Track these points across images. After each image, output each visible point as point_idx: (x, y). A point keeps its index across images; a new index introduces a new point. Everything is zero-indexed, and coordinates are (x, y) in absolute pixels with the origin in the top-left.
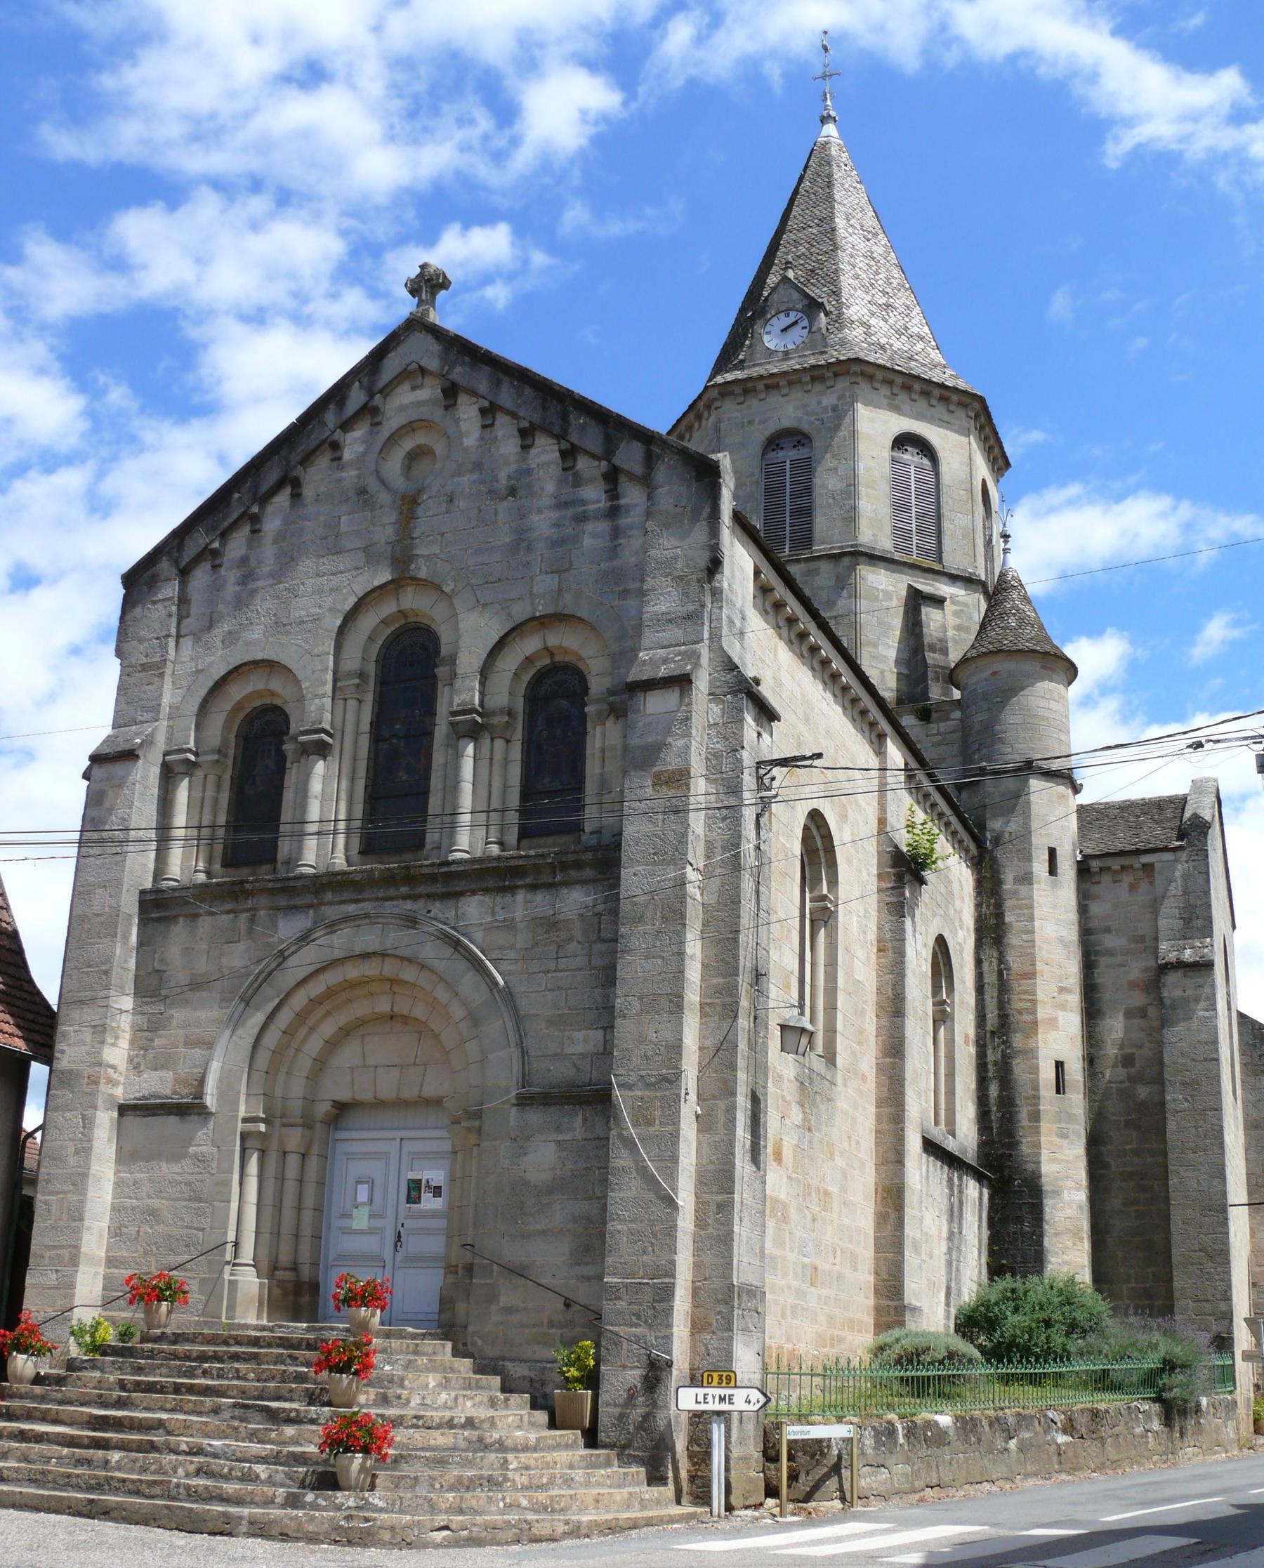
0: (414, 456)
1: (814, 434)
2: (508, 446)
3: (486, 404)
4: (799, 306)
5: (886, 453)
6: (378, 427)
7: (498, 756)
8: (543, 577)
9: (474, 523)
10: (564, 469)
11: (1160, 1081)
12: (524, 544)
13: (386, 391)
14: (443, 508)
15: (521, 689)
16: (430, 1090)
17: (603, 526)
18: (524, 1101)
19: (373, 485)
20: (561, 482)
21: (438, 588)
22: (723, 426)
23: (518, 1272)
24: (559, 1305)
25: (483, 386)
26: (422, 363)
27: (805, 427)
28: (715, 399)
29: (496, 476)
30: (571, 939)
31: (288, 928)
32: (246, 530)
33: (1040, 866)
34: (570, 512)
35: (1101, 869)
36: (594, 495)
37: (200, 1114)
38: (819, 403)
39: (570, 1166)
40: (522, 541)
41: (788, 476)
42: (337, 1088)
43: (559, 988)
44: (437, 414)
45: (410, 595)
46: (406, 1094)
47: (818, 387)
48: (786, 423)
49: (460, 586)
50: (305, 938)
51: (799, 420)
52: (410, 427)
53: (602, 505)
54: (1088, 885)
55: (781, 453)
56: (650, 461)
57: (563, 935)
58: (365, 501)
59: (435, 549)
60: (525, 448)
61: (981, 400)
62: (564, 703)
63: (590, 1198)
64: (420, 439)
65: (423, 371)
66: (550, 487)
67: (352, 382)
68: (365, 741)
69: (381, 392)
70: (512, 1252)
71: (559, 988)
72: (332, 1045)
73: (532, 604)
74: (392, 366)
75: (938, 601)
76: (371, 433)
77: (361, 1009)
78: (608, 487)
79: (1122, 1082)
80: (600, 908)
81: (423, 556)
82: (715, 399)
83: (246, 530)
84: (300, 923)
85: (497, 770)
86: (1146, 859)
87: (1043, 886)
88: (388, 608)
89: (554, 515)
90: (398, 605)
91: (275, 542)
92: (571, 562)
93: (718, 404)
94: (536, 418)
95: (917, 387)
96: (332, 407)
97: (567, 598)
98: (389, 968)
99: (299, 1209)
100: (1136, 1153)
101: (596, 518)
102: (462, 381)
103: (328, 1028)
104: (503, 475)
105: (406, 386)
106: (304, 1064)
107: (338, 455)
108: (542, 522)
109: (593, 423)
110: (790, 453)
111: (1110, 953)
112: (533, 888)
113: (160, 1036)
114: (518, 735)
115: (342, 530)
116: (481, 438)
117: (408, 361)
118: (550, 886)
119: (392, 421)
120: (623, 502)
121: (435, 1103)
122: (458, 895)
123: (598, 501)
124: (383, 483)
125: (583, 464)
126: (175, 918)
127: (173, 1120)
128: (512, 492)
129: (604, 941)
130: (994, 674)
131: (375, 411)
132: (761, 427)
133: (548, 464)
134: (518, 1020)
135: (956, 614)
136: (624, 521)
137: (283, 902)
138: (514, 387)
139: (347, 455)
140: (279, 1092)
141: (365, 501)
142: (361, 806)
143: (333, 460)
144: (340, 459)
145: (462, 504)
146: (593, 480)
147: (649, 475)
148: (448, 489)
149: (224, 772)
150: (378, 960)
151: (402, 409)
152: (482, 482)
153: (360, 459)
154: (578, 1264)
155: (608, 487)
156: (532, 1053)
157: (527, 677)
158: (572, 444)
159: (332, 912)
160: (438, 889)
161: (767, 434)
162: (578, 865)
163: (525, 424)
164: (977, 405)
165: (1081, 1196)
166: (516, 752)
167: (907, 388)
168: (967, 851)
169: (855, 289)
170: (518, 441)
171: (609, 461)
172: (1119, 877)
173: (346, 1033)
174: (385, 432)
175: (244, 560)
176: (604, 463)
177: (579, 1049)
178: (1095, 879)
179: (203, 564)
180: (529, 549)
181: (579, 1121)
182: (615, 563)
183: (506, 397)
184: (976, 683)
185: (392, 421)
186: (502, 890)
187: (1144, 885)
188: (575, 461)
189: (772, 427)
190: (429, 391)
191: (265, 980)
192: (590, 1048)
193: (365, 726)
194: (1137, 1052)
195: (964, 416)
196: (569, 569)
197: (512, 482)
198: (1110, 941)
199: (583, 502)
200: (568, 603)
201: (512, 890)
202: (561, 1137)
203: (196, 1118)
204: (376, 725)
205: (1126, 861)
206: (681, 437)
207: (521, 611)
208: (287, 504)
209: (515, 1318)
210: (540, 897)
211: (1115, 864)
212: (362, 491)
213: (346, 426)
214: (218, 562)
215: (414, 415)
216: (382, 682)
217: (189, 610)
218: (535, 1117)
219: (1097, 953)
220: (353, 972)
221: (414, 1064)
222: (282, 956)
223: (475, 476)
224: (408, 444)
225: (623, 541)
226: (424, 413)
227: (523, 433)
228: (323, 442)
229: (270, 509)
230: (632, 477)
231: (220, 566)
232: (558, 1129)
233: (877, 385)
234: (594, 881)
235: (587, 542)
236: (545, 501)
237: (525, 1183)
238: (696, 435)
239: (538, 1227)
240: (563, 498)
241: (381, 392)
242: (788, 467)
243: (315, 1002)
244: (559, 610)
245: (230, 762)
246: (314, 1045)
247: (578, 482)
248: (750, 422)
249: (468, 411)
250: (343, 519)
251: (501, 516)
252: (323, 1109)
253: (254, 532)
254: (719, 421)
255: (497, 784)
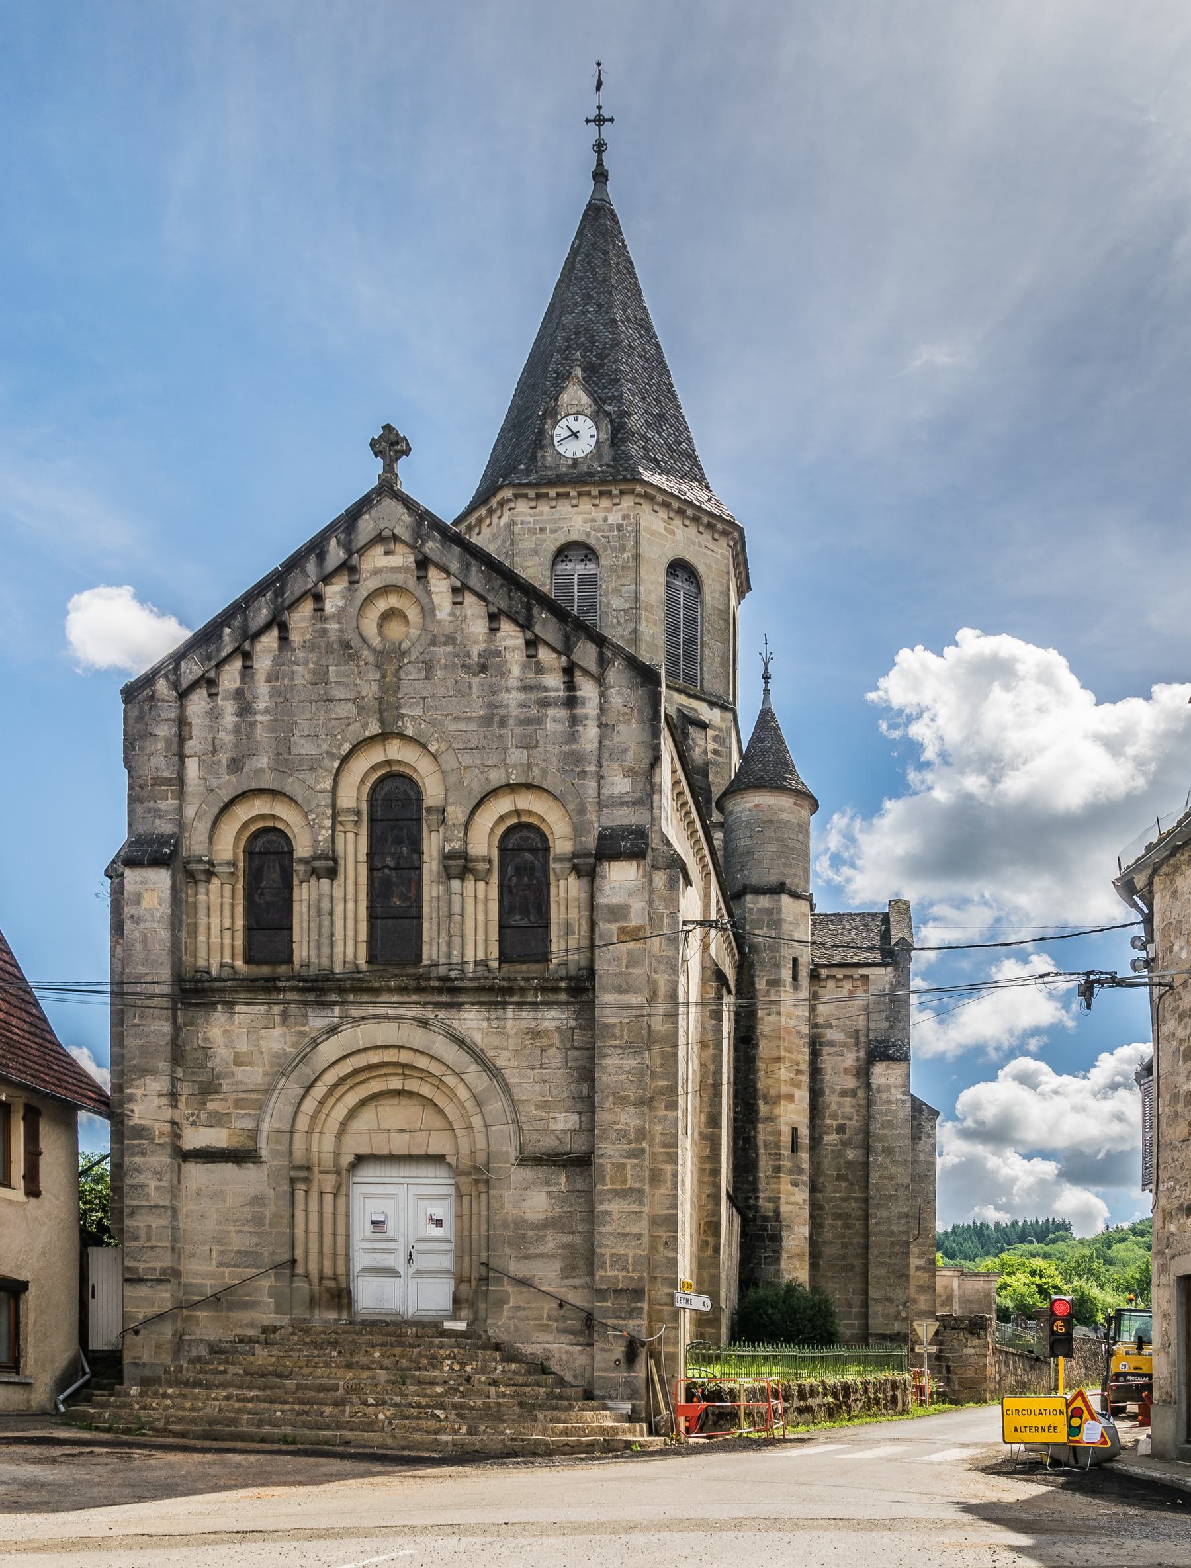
0: (389, 615)
1: (600, 551)
2: (479, 627)
3: (458, 583)
4: (588, 412)
5: (662, 578)
6: (356, 586)
7: (481, 896)
8: (514, 750)
9: (451, 693)
10: (528, 656)
11: (867, 1149)
12: (496, 719)
13: (362, 551)
14: (423, 675)
15: (496, 842)
16: (433, 1150)
17: (563, 713)
18: (522, 1162)
19: (356, 643)
20: (525, 667)
21: (425, 747)
22: (517, 529)
23: (523, 1282)
24: (555, 1305)
25: (454, 566)
26: (396, 531)
27: (592, 542)
28: (509, 500)
29: (468, 652)
30: (552, 1045)
31: (317, 1021)
32: (238, 664)
33: (786, 974)
34: (533, 696)
35: (829, 977)
36: (554, 682)
37: (255, 1163)
38: (606, 519)
39: (558, 1209)
40: (494, 718)
41: (576, 591)
42: (355, 1145)
43: (544, 1082)
44: (412, 583)
45: (396, 747)
46: (415, 1151)
47: (605, 503)
48: (575, 536)
49: (443, 748)
50: (333, 1030)
51: (588, 534)
52: (384, 590)
53: (561, 693)
54: (816, 989)
55: (570, 566)
56: (603, 662)
57: (545, 1042)
58: (350, 656)
59: (418, 711)
60: (494, 630)
61: (741, 531)
62: (528, 856)
63: (573, 1233)
64: (393, 601)
65: (395, 538)
66: (516, 671)
67: (328, 539)
68: (363, 870)
69: (357, 552)
70: (516, 1268)
71: (544, 1082)
72: (353, 1113)
73: (507, 772)
74: (366, 526)
75: (704, 726)
76: (349, 589)
77: (376, 1086)
78: (566, 679)
79: (836, 1145)
80: (573, 1023)
81: (408, 716)
82: (509, 500)
83: (238, 664)
84: (333, 1016)
85: (481, 906)
86: (863, 971)
87: (787, 989)
88: (375, 755)
89: (521, 696)
90: (386, 755)
91: (268, 681)
92: (537, 741)
93: (512, 505)
94: (503, 605)
95: (690, 512)
96: (313, 558)
97: (536, 772)
98: (404, 1057)
99: (335, 1235)
100: (844, 1199)
101: (556, 705)
102: (436, 557)
103: (352, 1099)
104: (475, 651)
105: (379, 550)
106: (333, 1125)
107: (320, 606)
108: (512, 699)
109: (554, 619)
110: (578, 567)
111: (832, 1044)
112: (520, 1005)
113: (212, 1100)
114: (495, 878)
115: (331, 680)
116: (452, 614)
117: (382, 526)
118: (534, 1005)
119: (368, 585)
120: (578, 693)
121: (439, 1159)
122: (459, 1006)
123: (558, 690)
124: (364, 640)
125: (543, 654)
126: (215, 1004)
127: (229, 1168)
128: (483, 668)
129: (576, 1048)
130: (757, 806)
131: (353, 570)
132: (552, 536)
133: (514, 649)
134: (513, 1103)
135: (715, 739)
136: (579, 711)
137: (311, 997)
138: (482, 572)
139: (329, 607)
140: (314, 1148)
141: (350, 656)
142: (365, 923)
143: (315, 610)
144: (322, 610)
145: (440, 674)
146: (552, 670)
147: (603, 675)
148: (427, 657)
149: (237, 882)
150: (396, 1051)
151: (377, 572)
152: (456, 656)
153: (339, 615)
154: (567, 1277)
155: (566, 679)
156: (525, 1127)
157: (499, 831)
158: (536, 636)
159: (355, 1012)
160: (445, 998)
161: (558, 544)
162: (556, 990)
163: (494, 609)
164: (736, 535)
165: (805, 1230)
166: (494, 893)
167: (681, 512)
168: (733, 956)
169: (633, 395)
170: (485, 622)
171: (568, 657)
172: (839, 984)
173: (363, 1103)
174: (364, 591)
175: (239, 694)
176: (564, 658)
177: (561, 1126)
178: (822, 984)
179: (198, 691)
180: (502, 723)
181: (563, 1179)
182: (574, 747)
183: (476, 578)
184: (741, 812)
185: (368, 585)
186: (494, 1004)
187: (860, 992)
188: (537, 650)
189: (562, 539)
190: (402, 558)
191: (301, 1061)
192: (569, 1126)
193: (362, 857)
194: (848, 1123)
195: (725, 545)
196: (536, 747)
197: (483, 660)
198: (830, 1035)
199: (546, 689)
200: (535, 776)
201: (504, 1005)
202: (550, 1189)
203: (251, 1165)
204: (370, 855)
205: (848, 971)
206: (470, 529)
207: (496, 777)
208: (276, 645)
209: (522, 1314)
210: (525, 1013)
211: (840, 973)
212: (346, 646)
213: (327, 579)
214: (214, 691)
215: (391, 579)
216: (372, 820)
217: (190, 732)
218: (528, 1174)
219: (821, 1044)
220: (374, 1058)
221: (421, 1130)
222: (315, 1043)
223: (449, 649)
224: (382, 605)
225: (580, 728)
226: (399, 579)
227: (493, 617)
228: (305, 593)
229: (259, 647)
230: (586, 672)
231: (217, 695)
232: (548, 1183)
233: (657, 508)
234: (568, 1003)
235: (550, 726)
236: (513, 682)
237: (525, 1221)
238: (485, 530)
239: (537, 1251)
240: (528, 682)
241: (357, 552)
242: (576, 580)
243: (342, 1080)
244: (530, 781)
245: (241, 873)
246: (341, 1111)
247: (540, 669)
248: (542, 530)
249: (440, 585)
250: (331, 669)
251: (474, 690)
252: (346, 1160)
253: (245, 667)
254: (513, 523)
255: (481, 918)
